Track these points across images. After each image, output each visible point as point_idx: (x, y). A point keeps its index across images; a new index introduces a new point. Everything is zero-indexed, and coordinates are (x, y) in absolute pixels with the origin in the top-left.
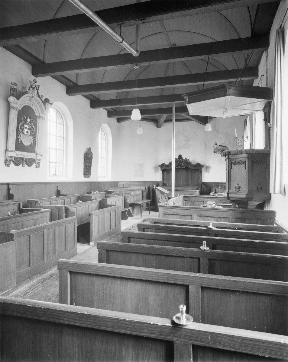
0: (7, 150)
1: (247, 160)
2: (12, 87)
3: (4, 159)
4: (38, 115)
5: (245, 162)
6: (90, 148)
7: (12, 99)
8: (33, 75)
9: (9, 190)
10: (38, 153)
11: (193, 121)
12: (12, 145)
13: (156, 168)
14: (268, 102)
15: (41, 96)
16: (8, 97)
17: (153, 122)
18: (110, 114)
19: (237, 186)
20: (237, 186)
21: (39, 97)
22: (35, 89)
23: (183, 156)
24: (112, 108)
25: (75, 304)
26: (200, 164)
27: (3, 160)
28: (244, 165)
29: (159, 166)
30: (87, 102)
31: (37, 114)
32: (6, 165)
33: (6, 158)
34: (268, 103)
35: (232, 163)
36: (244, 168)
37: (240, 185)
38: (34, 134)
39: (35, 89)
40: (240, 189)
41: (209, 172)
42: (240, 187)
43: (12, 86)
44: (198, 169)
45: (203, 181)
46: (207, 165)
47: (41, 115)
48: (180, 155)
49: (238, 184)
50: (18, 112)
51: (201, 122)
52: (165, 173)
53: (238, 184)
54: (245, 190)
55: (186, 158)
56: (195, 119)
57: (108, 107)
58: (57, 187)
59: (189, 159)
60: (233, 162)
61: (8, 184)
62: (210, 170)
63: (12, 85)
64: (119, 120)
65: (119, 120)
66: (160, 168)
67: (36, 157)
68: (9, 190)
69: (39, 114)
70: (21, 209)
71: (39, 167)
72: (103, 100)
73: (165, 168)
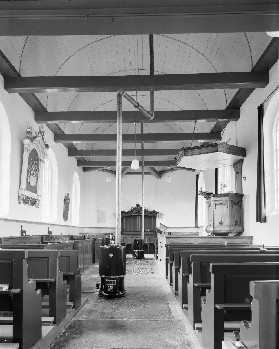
1: (228, 202)
2: (28, 131)
3: (18, 197)
4: (40, 158)
5: (227, 203)
6: (68, 194)
7: (27, 142)
10: (39, 194)
11: (152, 174)
12: (24, 185)
14: (242, 159)
15: (45, 142)
16: (24, 140)
18: (80, 163)
21: (43, 141)
22: (42, 134)
24: (83, 158)
25: (196, 285)
26: (156, 211)
27: (17, 198)
30: (65, 151)
31: (39, 158)
32: (20, 203)
33: (19, 196)
38: (37, 177)
39: (42, 134)
40: (223, 224)
41: (162, 218)
43: (27, 129)
44: (153, 216)
47: (42, 159)
49: (221, 221)
50: (29, 154)
52: (124, 220)
53: (221, 221)
57: (77, 157)
60: (217, 203)
62: (164, 217)
63: (28, 128)
64: (85, 170)
65: (85, 170)
69: (41, 158)
71: (38, 207)
72: (81, 149)
73: (125, 215)
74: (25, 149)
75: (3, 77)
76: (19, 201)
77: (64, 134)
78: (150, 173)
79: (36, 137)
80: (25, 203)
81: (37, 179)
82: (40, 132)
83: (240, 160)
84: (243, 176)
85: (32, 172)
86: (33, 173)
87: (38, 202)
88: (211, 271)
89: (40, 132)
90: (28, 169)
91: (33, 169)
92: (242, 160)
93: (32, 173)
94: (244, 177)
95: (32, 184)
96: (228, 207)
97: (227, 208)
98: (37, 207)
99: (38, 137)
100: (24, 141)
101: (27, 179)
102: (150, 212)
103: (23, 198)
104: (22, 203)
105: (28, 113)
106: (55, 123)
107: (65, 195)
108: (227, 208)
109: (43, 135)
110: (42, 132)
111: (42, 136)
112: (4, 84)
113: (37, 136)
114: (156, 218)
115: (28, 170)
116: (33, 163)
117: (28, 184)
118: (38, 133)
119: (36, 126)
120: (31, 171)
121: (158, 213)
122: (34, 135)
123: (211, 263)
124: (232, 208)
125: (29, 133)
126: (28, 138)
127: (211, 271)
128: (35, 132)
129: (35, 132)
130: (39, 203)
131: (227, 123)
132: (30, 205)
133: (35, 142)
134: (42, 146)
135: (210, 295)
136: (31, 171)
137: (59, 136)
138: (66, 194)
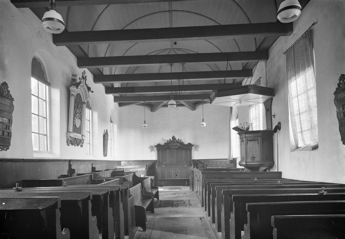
0: (68, 131)
4: (83, 101)
8: (78, 66)
9: (70, 166)
11: (185, 106)
12: (71, 129)
13: (152, 148)
14: (271, 98)
17: (148, 107)
19: (252, 156)
20: (252, 156)
22: (85, 79)
23: (176, 137)
28: (257, 142)
29: (155, 146)
32: (68, 145)
34: (270, 99)
35: (248, 140)
36: (257, 144)
37: (254, 156)
40: (254, 158)
41: (198, 151)
42: (255, 157)
43: (73, 77)
45: (192, 159)
46: (196, 144)
48: (174, 136)
49: (253, 155)
51: (191, 108)
54: (258, 158)
55: (179, 139)
56: (188, 105)
58: (92, 164)
59: (181, 140)
61: (70, 161)
66: (155, 148)
67: (82, 138)
68: (70, 166)
70: (93, 180)
71: (83, 146)
74: (71, 95)
75: (75, 58)
76: (67, 142)
77: (103, 74)
78: (184, 105)
79: (80, 83)
80: (72, 144)
81: (81, 121)
82: (83, 77)
83: (270, 98)
84: (273, 114)
85: (77, 115)
86: (78, 116)
87: (83, 142)
88: (247, 209)
89: (84, 78)
90: (74, 112)
91: (78, 112)
92: (272, 99)
93: (77, 116)
94: (273, 115)
95: (78, 126)
96: (259, 143)
97: (258, 144)
98: (82, 146)
99: (81, 82)
100: (70, 88)
101: (74, 122)
102: (185, 145)
103: (71, 140)
104: (70, 145)
105: (73, 60)
106: (97, 67)
107: (104, 131)
108: (258, 144)
109: (86, 80)
110: (84, 77)
111: (84, 81)
112: (52, 38)
113: (81, 81)
114: (191, 151)
115: (74, 114)
116: (78, 107)
117: (75, 126)
118: (82, 79)
119: (79, 71)
120: (76, 114)
121: (193, 145)
122: (78, 81)
123: (247, 204)
124: (263, 143)
125: (74, 80)
126: (74, 85)
127: (247, 209)
128: (79, 78)
129: (79, 78)
130: (83, 143)
131: (256, 64)
132: (76, 145)
133: (79, 87)
134: (85, 89)
135: (247, 227)
136: (76, 115)
137: (98, 78)
138: (105, 130)
